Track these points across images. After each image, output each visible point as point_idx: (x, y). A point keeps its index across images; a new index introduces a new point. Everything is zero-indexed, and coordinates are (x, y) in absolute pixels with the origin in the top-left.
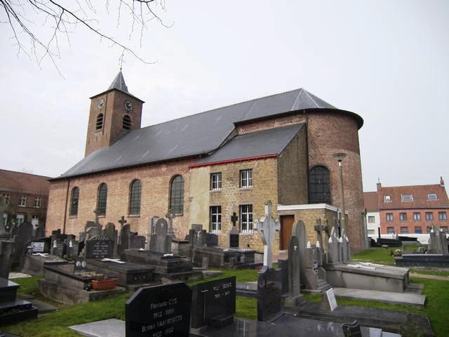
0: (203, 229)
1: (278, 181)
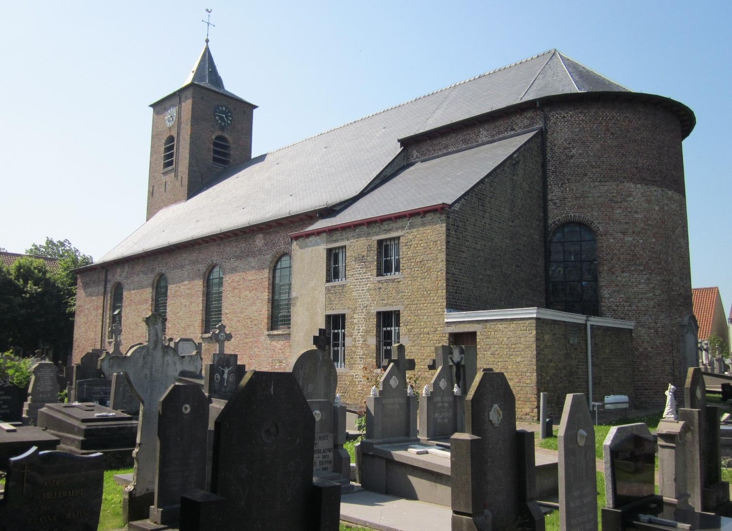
0: (239, 363)
1: (447, 261)
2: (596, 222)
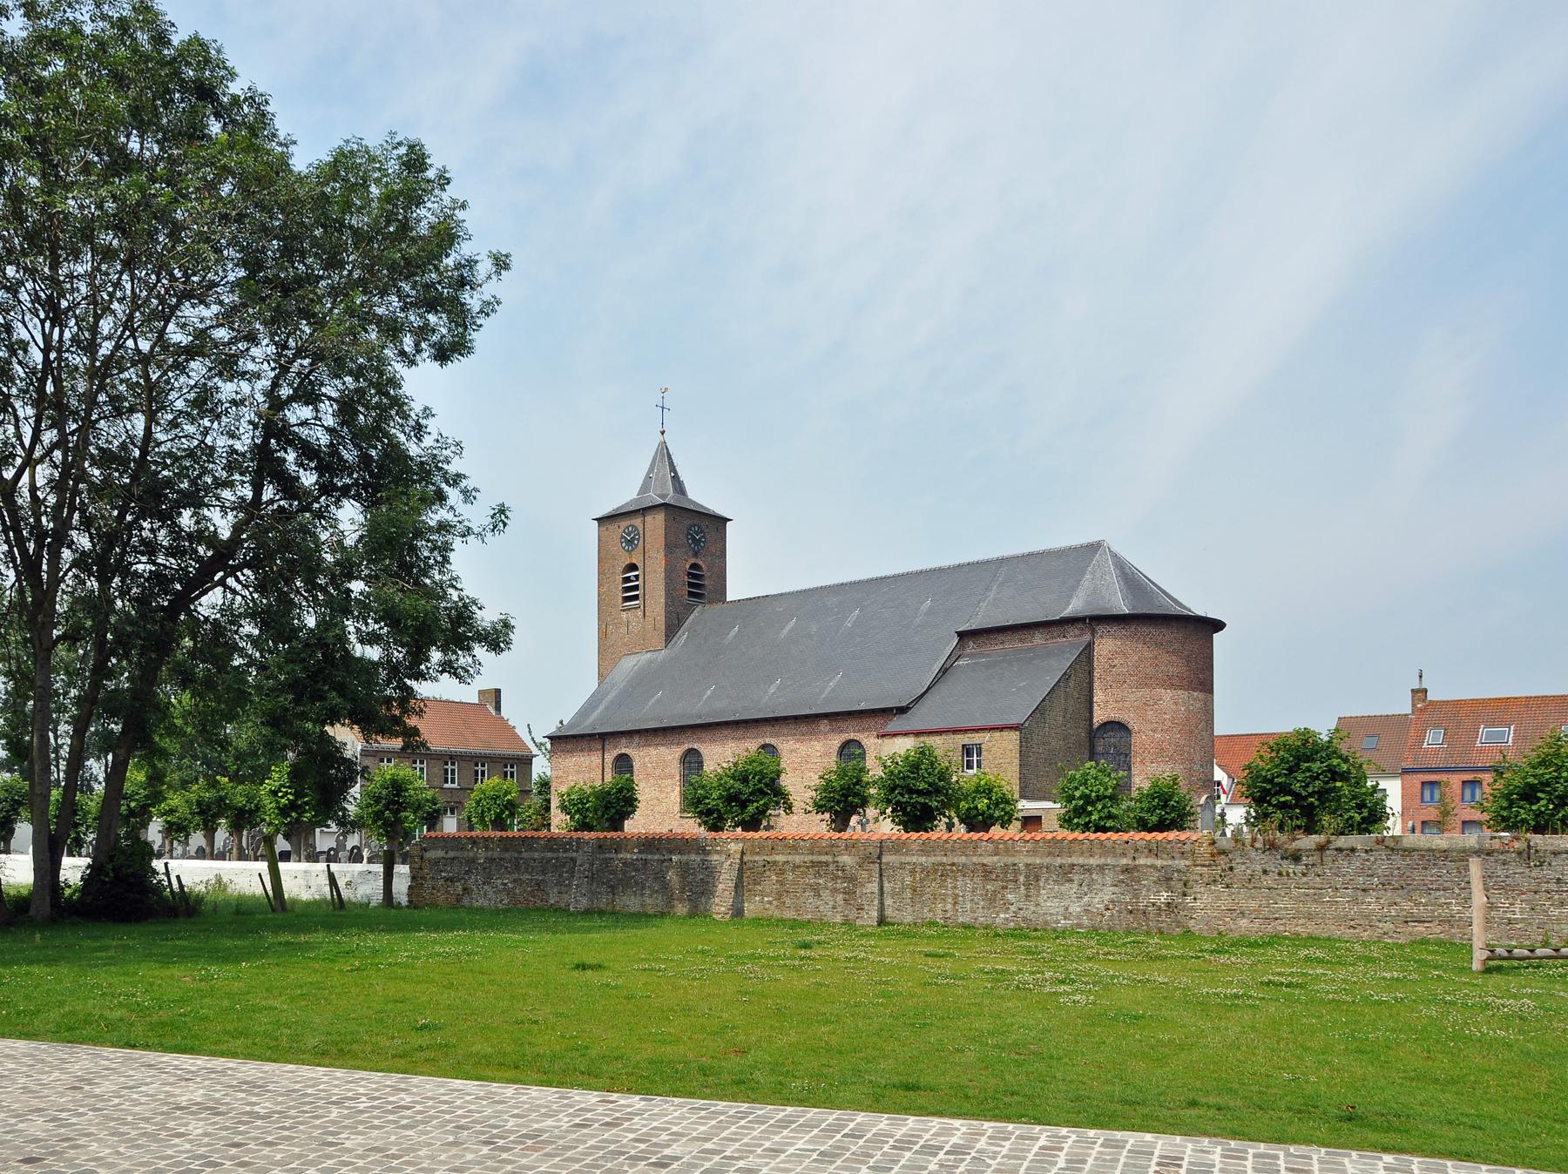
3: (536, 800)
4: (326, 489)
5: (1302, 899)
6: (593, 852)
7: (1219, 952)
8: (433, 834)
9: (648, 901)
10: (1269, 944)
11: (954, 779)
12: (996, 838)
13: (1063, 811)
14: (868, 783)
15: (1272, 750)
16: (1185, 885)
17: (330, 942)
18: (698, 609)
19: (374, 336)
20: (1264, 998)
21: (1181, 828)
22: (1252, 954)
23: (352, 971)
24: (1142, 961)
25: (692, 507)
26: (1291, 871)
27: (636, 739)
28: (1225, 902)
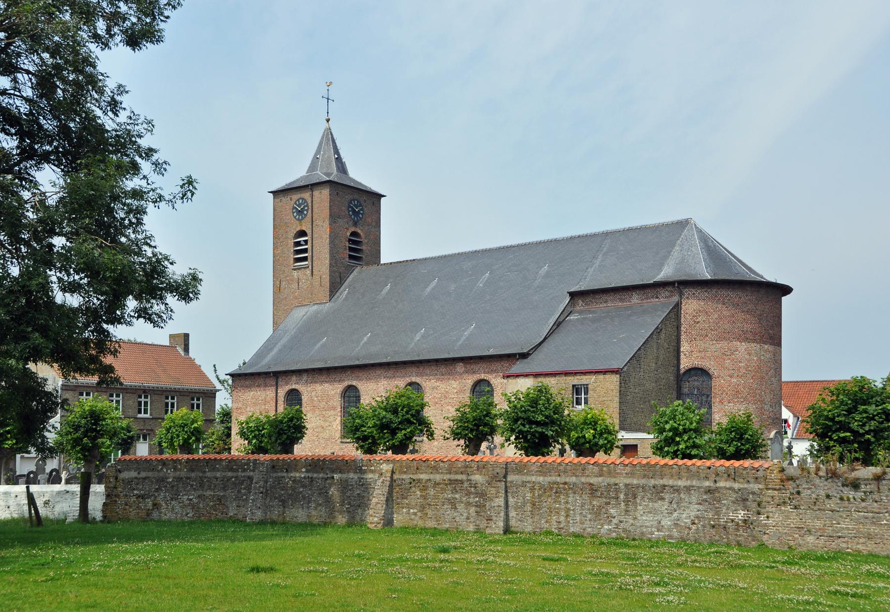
2: (712, 368)
3: (219, 428)
4: (27, 153)
5: (862, 521)
6: (267, 472)
7: (790, 564)
8: (127, 457)
9: (314, 513)
10: (834, 558)
11: (566, 412)
12: (601, 462)
13: (656, 441)
14: (496, 415)
15: (833, 394)
16: (759, 505)
17: (26, 556)
18: (356, 270)
19: (67, 17)
20: (832, 606)
21: (755, 458)
22: (819, 566)
23: (47, 581)
24: (724, 568)
25: (352, 184)
26: (851, 496)
27: (305, 377)
28: (794, 520)
